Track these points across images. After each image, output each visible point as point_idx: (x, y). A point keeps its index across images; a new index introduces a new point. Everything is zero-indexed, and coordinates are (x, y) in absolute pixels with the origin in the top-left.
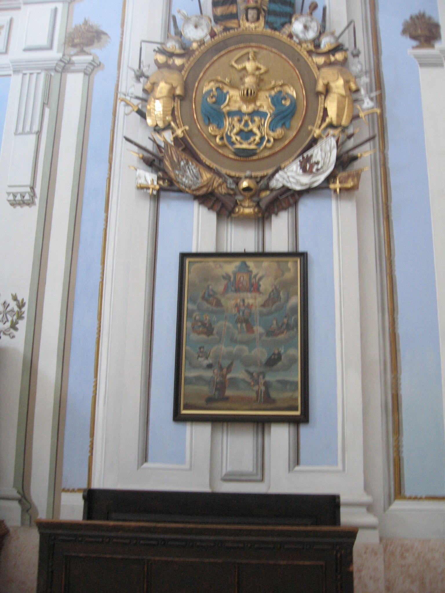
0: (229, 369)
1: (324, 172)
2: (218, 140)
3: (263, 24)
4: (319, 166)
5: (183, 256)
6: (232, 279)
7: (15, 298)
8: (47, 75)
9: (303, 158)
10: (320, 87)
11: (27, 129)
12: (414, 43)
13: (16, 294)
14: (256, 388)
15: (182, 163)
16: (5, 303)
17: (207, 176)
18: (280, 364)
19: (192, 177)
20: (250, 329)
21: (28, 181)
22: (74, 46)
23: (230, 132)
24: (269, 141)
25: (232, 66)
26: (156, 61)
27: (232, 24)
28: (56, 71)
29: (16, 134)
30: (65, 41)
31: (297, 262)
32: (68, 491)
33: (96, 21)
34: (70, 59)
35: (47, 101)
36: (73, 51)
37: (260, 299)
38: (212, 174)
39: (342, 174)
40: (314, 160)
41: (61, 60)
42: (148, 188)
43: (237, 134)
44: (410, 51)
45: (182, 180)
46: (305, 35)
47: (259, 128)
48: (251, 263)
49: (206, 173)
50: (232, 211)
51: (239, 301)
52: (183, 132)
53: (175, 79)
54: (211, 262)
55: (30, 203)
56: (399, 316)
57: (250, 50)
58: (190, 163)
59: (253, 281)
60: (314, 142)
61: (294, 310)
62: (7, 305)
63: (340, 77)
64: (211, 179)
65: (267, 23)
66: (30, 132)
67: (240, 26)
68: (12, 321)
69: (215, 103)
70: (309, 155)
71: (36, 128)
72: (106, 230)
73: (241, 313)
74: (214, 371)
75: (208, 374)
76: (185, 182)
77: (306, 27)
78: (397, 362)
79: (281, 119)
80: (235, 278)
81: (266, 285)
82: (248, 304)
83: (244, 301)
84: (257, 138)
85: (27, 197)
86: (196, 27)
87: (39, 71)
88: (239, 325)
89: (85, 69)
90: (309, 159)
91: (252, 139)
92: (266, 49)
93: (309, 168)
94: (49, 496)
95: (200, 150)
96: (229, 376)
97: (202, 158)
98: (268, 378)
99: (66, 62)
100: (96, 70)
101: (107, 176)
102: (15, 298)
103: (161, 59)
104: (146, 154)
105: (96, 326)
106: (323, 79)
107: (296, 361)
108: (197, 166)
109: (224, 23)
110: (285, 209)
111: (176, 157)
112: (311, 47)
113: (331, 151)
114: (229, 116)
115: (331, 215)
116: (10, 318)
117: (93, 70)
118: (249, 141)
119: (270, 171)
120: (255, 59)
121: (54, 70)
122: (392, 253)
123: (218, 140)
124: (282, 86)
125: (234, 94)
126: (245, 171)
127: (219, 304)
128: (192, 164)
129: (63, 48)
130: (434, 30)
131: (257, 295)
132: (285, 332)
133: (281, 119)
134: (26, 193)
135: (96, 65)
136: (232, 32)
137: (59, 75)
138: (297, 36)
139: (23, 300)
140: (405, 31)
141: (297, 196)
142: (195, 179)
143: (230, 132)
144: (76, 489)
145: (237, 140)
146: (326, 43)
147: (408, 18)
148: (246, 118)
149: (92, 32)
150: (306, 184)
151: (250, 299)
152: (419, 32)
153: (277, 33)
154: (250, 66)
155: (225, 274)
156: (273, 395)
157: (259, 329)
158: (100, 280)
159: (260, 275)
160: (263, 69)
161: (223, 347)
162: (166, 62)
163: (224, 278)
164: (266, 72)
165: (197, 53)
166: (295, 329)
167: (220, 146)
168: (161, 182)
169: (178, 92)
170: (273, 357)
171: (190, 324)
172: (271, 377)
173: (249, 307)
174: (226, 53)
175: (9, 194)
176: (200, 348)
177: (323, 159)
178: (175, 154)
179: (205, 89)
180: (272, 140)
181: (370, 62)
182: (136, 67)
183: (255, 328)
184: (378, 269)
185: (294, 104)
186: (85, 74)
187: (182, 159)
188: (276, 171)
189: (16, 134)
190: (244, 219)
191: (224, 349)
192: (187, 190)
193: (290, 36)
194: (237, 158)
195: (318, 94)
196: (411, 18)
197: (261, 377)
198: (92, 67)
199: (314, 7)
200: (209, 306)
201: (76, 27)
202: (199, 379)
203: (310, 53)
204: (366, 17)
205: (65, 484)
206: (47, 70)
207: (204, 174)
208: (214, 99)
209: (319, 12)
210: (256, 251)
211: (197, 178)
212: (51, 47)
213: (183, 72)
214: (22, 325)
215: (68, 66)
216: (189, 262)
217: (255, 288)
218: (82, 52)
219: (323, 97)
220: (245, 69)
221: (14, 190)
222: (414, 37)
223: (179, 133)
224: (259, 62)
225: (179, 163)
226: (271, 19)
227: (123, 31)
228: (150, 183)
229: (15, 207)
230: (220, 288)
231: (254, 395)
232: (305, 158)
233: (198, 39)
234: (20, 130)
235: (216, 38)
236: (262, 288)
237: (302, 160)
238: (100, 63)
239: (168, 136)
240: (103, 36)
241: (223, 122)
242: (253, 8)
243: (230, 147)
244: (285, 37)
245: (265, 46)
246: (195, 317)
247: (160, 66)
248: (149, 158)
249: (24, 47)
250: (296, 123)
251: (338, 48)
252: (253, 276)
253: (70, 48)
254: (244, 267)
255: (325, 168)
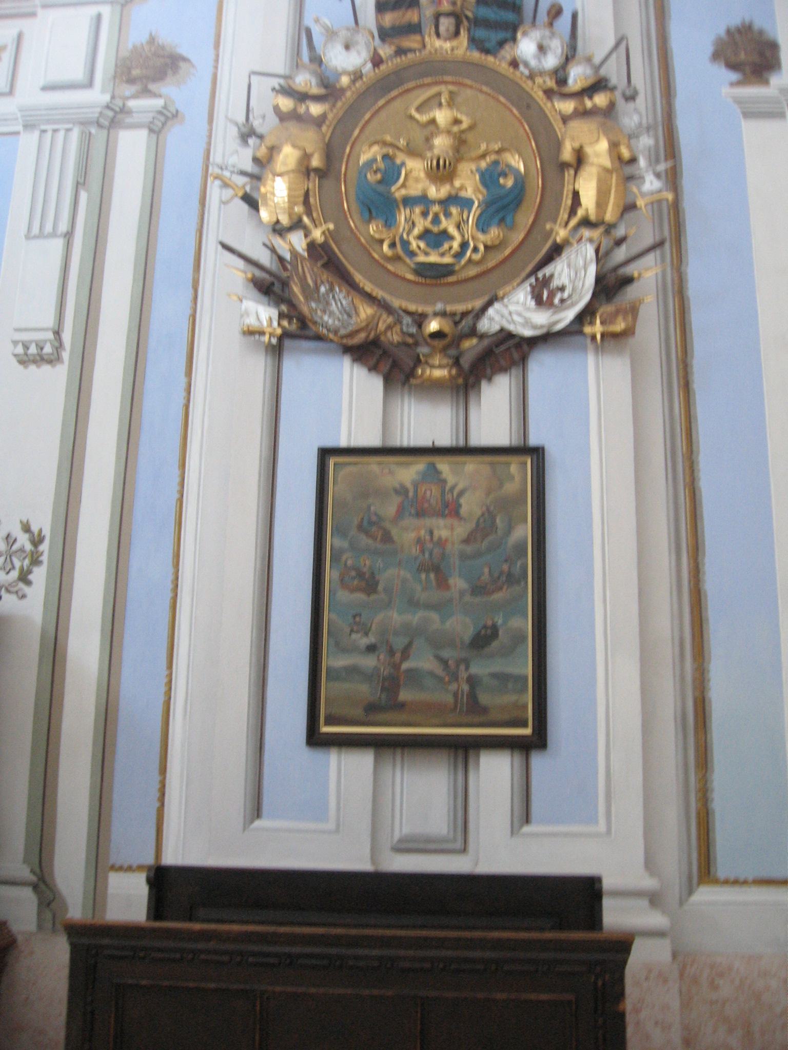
0: (406, 653)
1: (573, 305)
2: (385, 247)
3: (465, 43)
4: (566, 295)
5: (325, 454)
6: (411, 494)
7: (26, 528)
8: (83, 133)
9: (537, 279)
10: (567, 154)
11: (49, 228)
12: (734, 76)
13: (28, 521)
14: (453, 687)
15: (323, 289)
16: (8, 536)
17: (366, 311)
18: (495, 644)
19: (341, 313)
20: (443, 583)
21: (49, 321)
22: (131, 81)
23: (408, 235)
24: (475, 249)
25: (411, 117)
26: (276, 109)
27: (411, 42)
28: (100, 125)
29: (28, 237)
30: (116, 72)
31: (526, 464)
32: (120, 869)
33: (170, 37)
34: (124, 105)
35: (83, 178)
36: (129, 90)
37: (461, 530)
38: (375, 308)
39: (606, 309)
40: (556, 283)
41: (108, 107)
42: (262, 333)
43: (420, 237)
44: (726, 90)
45: (321, 318)
46: (540, 61)
47: (458, 227)
48: (444, 466)
49: (365, 306)
50: (411, 374)
51: (423, 532)
52: (323, 233)
53: (311, 140)
54: (373, 464)
55: (53, 360)
56: (707, 560)
57: (443, 88)
58: (337, 289)
59: (449, 497)
60: (556, 251)
61: (520, 549)
62: (12, 541)
63: (601, 136)
64: (373, 316)
65: (473, 41)
66: (53, 235)
67: (424, 46)
68: (22, 569)
69: (380, 182)
70: (547, 275)
71: (63, 227)
72: (187, 407)
73: (427, 555)
74: (378, 657)
75: (369, 662)
76: (327, 323)
77: (542, 49)
78: (702, 642)
79: (497, 211)
80: (416, 491)
81: (471, 505)
82: (440, 538)
83: (431, 533)
84: (456, 245)
85: (48, 349)
86: (347, 47)
87: (69, 126)
88: (423, 576)
89: (151, 123)
90: (546, 281)
91: (446, 246)
92: (471, 87)
93: (548, 298)
94: (87, 878)
95: (354, 266)
96: (405, 666)
97: (357, 280)
98: (475, 670)
99: (117, 109)
100: (169, 123)
101: (189, 312)
102: (26, 528)
103: (286, 104)
104: (259, 274)
105: (171, 577)
106: (573, 139)
107: (524, 638)
108: (348, 294)
109: (396, 41)
110: (504, 370)
111: (312, 278)
112: (551, 83)
113: (585, 268)
114: (405, 206)
115: (586, 381)
116: (17, 564)
117: (164, 124)
118: (442, 250)
119: (478, 303)
120: (451, 104)
121: (96, 125)
122: (694, 448)
123: (385, 247)
124: (499, 152)
125: (415, 167)
126: (434, 304)
127: (387, 538)
128: (341, 291)
129: (112, 85)
130: (768, 54)
131: (455, 522)
132: (505, 587)
133: (497, 211)
134: (45, 341)
135: (169, 115)
136: (410, 56)
137: (105, 132)
138: (526, 65)
139: (41, 531)
140: (717, 56)
141: (525, 347)
142: (345, 317)
143: (408, 235)
144: (135, 865)
145: (419, 247)
146: (577, 76)
147: (722, 32)
148: (436, 208)
149: (163, 57)
150: (542, 327)
151: (443, 529)
152: (742, 56)
153: (491, 59)
154: (442, 116)
155: (398, 486)
156: (484, 699)
157: (458, 583)
158: (177, 496)
159: (460, 486)
160: (466, 123)
161: (395, 615)
162: (295, 110)
163: (396, 491)
164: (471, 128)
165: (348, 94)
166: (523, 583)
167: (389, 259)
168: (285, 323)
169: (316, 162)
170: (483, 632)
171: (336, 575)
172: (480, 668)
173: (441, 543)
174: (401, 94)
175: (15, 343)
176: (354, 617)
177: (573, 282)
178: (310, 272)
179: (364, 158)
180: (482, 248)
181: (655, 110)
182: (241, 119)
183: (451, 581)
184: (670, 476)
185: (521, 184)
186: (151, 130)
187: (322, 282)
188: (489, 303)
189: (28, 237)
190: (433, 388)
191: (396, 617)
192: (331, 336)
193: (514, 64)
194: (420, 280)
195: (564, 166)
196: (729, 32)
197: (462, 667)
198: (162, 119)
199: (556, 12)
200: (370, 541)
201: (135, 47)
202: (353, 671)
203: (549, 93)
204: (648, 30)
205: (116, 858)
206: (84, 123)
207: (361, 308)
208: (379, 176)
209: (564, 22)
210: (454, 444)
211: (349, 316)
212: (90, 84)
213: (324, 128)
214: (39, 575)
215: (120, 116)
216: (334, 464)
217: (451, 509)
218: (146, 92)
219: (572, 172)
220: (433, 121)
221: (25, 336)
222: (732, 66)
223: (317, 235)
224: (458, 110)
225: (317, 289)
226: (481, 33)
227: (217, 56)
228: (265, 323)
229: (26, 367)
230: (390, 509)
231: (450, 699)
232: (541, 279)
233: (350, 68)
234: (36, 230)
235: (383, 67)
236: (463, 511)
237: (534, 284)
238: (177, 111)
239: (298, 241)
240: (182, 64)
241: (394, 217)
242: (448, 15)
243: (408, 261)
244: (504, 65)
245: (468, 82)
246: (346, 562)
247: (282, 117)
248: (263, 280)
249: (42, 83)
250: (525, 218)
251: (598, 85)
252: (447, 488)
253: (125, 85)
254: (433, 473)
255: (575, 298)
